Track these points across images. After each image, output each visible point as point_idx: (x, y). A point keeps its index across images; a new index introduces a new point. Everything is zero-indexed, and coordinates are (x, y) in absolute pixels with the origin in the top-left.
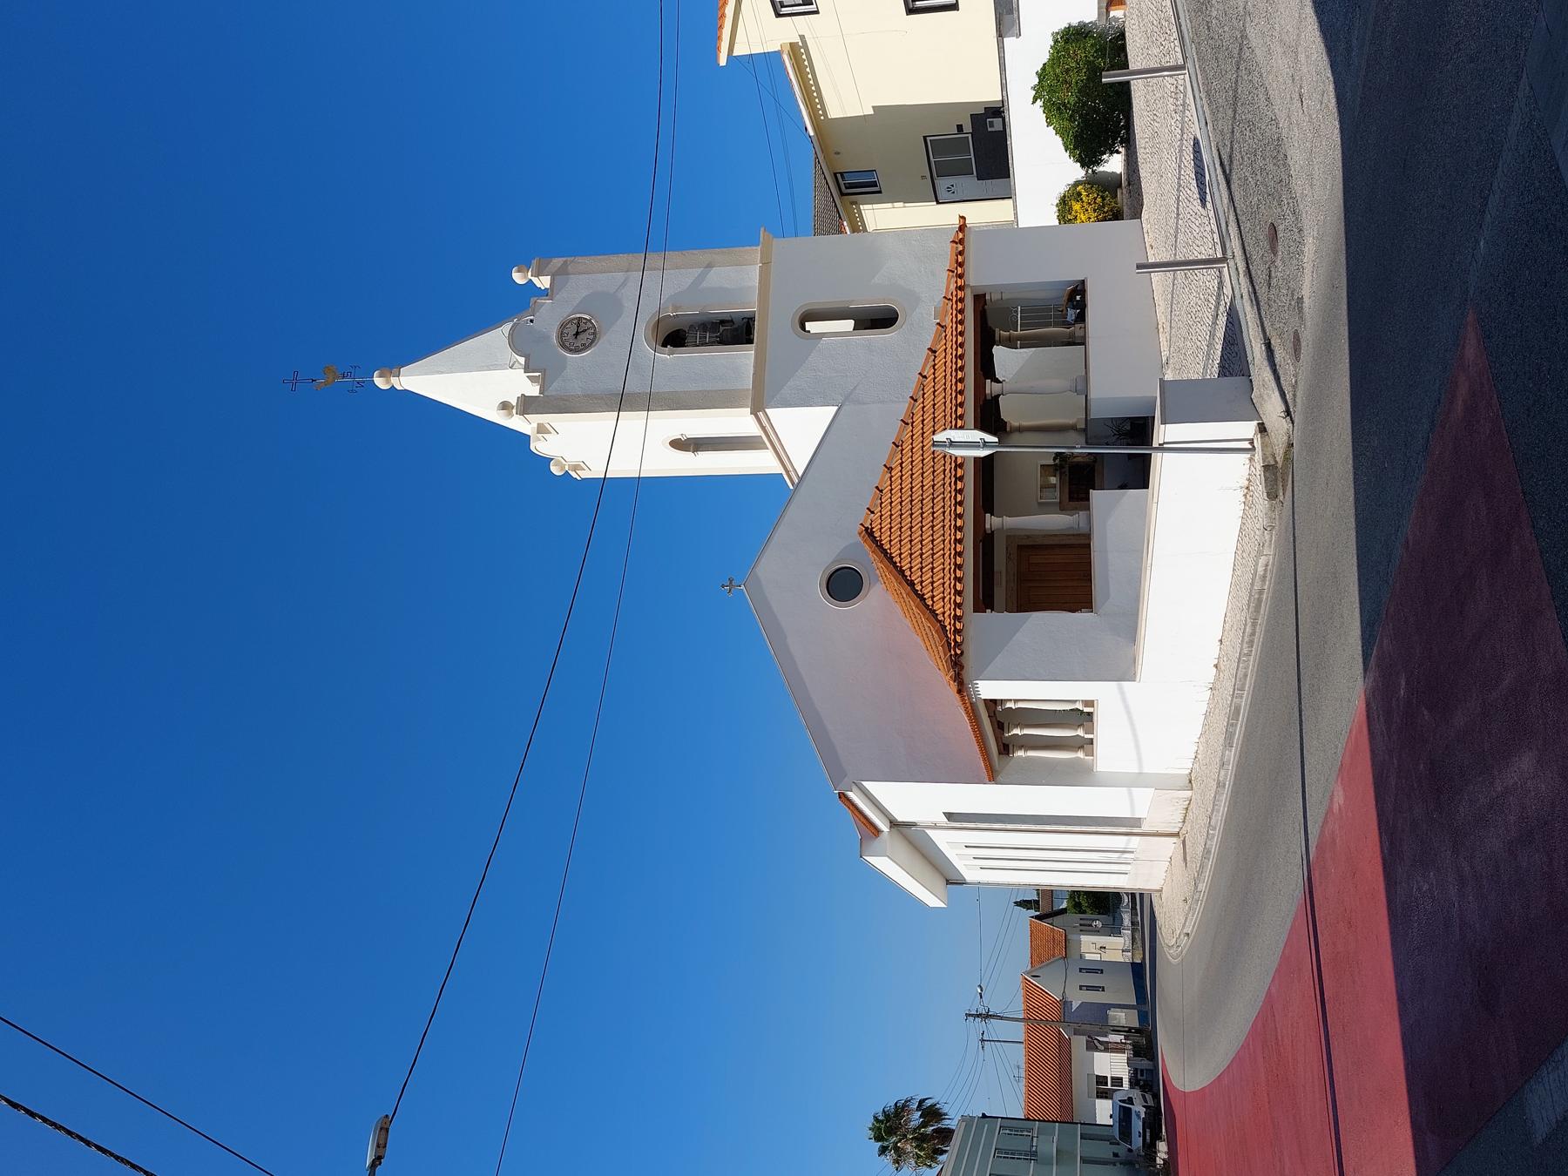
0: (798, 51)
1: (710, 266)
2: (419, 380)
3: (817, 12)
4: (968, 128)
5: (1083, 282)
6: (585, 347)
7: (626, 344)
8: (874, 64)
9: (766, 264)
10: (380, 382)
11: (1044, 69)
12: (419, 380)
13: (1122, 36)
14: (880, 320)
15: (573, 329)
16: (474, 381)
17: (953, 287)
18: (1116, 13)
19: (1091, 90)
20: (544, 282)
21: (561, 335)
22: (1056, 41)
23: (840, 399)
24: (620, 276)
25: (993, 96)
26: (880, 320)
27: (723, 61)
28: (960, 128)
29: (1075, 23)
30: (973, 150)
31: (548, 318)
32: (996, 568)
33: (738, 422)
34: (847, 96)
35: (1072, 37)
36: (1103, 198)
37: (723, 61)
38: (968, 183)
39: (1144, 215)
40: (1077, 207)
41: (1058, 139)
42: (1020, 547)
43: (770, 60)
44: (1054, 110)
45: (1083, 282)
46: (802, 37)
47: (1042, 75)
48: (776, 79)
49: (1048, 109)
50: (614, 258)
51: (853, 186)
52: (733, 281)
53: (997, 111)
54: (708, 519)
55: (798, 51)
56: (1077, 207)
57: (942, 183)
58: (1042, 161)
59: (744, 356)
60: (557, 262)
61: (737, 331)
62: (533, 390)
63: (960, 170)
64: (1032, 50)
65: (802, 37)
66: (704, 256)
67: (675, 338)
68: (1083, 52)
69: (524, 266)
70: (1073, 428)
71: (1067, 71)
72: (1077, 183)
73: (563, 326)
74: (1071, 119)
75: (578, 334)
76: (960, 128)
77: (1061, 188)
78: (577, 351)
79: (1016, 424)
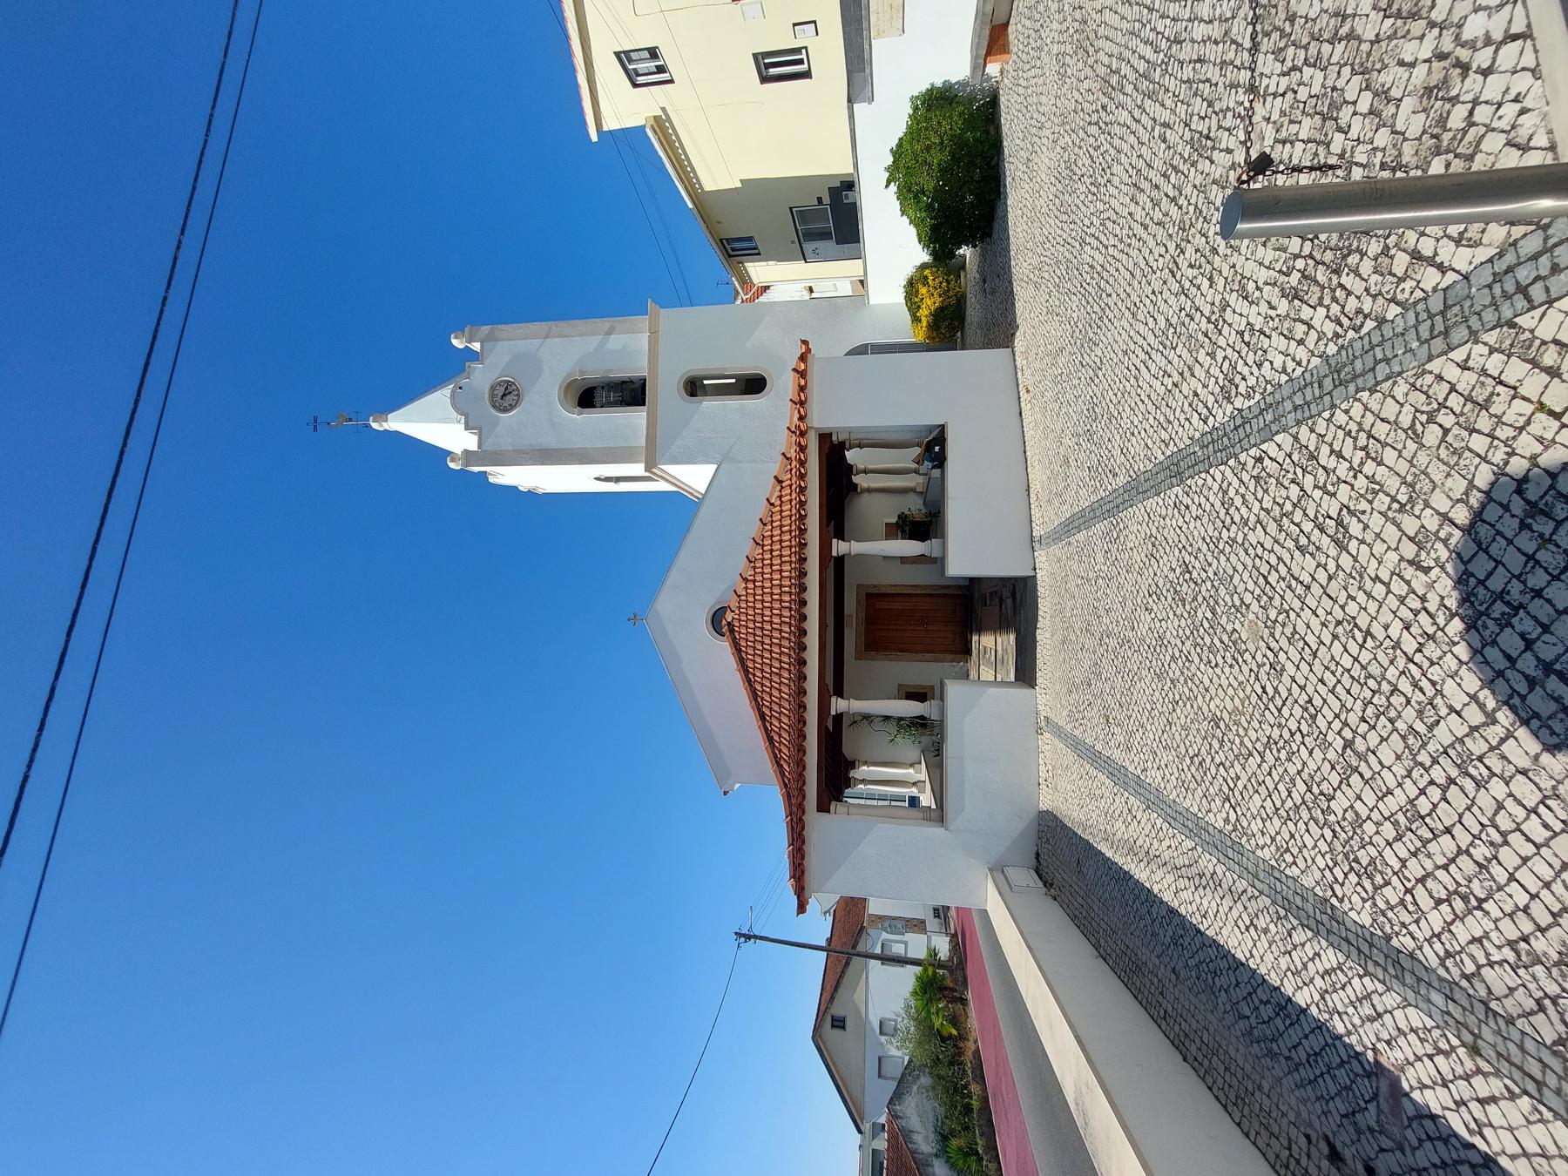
0: (662, 124)
1: (610, 332)
2: (400, 422)
3: (672, 81)
4: (827, 200)
5: (942, 428)
6: (512, 407)
7: (546, 407)
8: (740, 140)
9: (654, 333)
10: (375, 426)
11: (900, 145)
12: (400, 422)
13: (993, 102)
14: (753, 385)
15: (501, 391)
16: (436, 425)
17: (797, 416)
18: (993, 69)
19: (960, 171)
20: (476, 346)
21: (492, 396)
22: (916, 109)
23: (719, 457)
24: (537, 342)
25: (843, 168)
26: (753, 385)
27: (594, 138)
28: (820, 199)
29: (939, 84)
30: (830, 219)
31: (481, 377)
32: (846, 612)
33: (638, 469)
34: (718, 172)
35: (936, 101)
36: (948, 282)
37: (594, 138)
38: (828, 246)
39: (1019, 343)
40: (923, 290)
41: (913, 231)
42: (868, 595)
43: (631, 138)
44: (909, 196)
45: (942, 428)
46: (663, 109)
47: (897, 153)
48: (644, 155)
49: (901, 196)
50: (530, 325)
51: (737, 249)
52: (624, 348)
53: (849, 185)
54: (640, 531)
55: (662, 124)
56: (923, 290)
57: (809, 247)
58: (893, 244)
59: (634, 419)
60: (485, 329)
61: (632, 393)
62: (473, 447)
63: (823, 235)
64: (887, 121)
65: (663, 109)
66: (605, 323)
67: (587, 398)
68: (950, 124)
69: (459, 330)
70: (913, 490)
71: (928, 148)
72: (923, 266)
73: (493, 388)
74: (929, 207)
75: (506, 395)
76: (820, 199)
77: (908, 270)
78: (505, 410)
79: (865, 485)
